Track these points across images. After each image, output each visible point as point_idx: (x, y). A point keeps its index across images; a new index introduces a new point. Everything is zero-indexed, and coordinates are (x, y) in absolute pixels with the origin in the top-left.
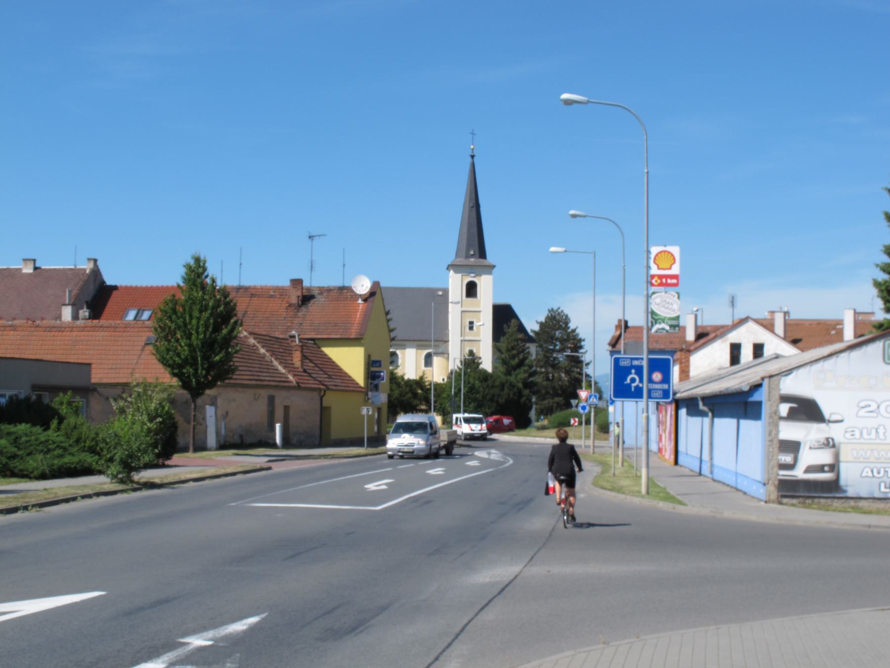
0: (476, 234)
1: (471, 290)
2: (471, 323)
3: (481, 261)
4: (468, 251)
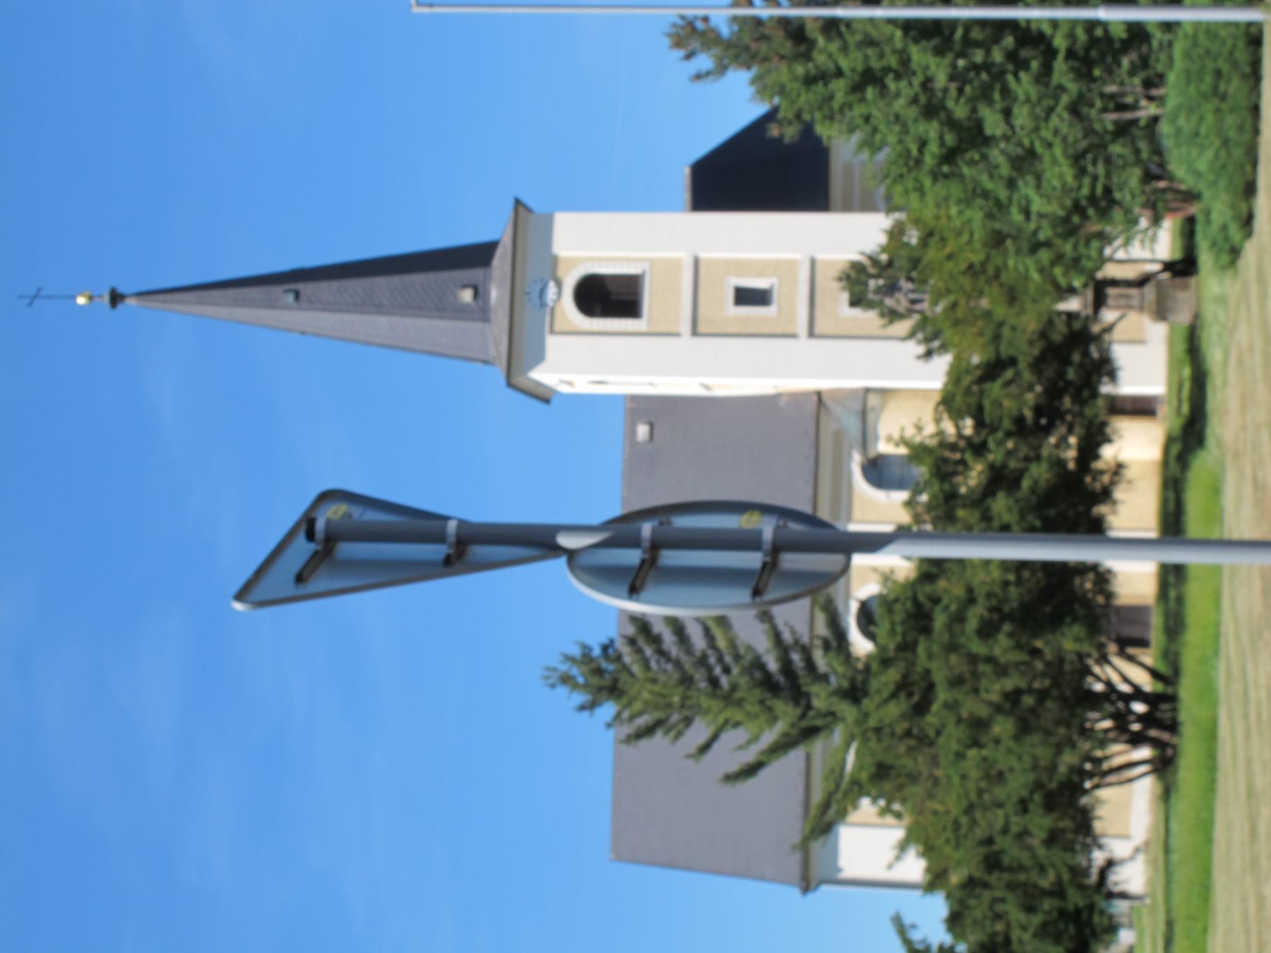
0: (396, 280)
1: (608, 297)
2: (746, 297)
3: (501, 261)
4: (461, 312)
